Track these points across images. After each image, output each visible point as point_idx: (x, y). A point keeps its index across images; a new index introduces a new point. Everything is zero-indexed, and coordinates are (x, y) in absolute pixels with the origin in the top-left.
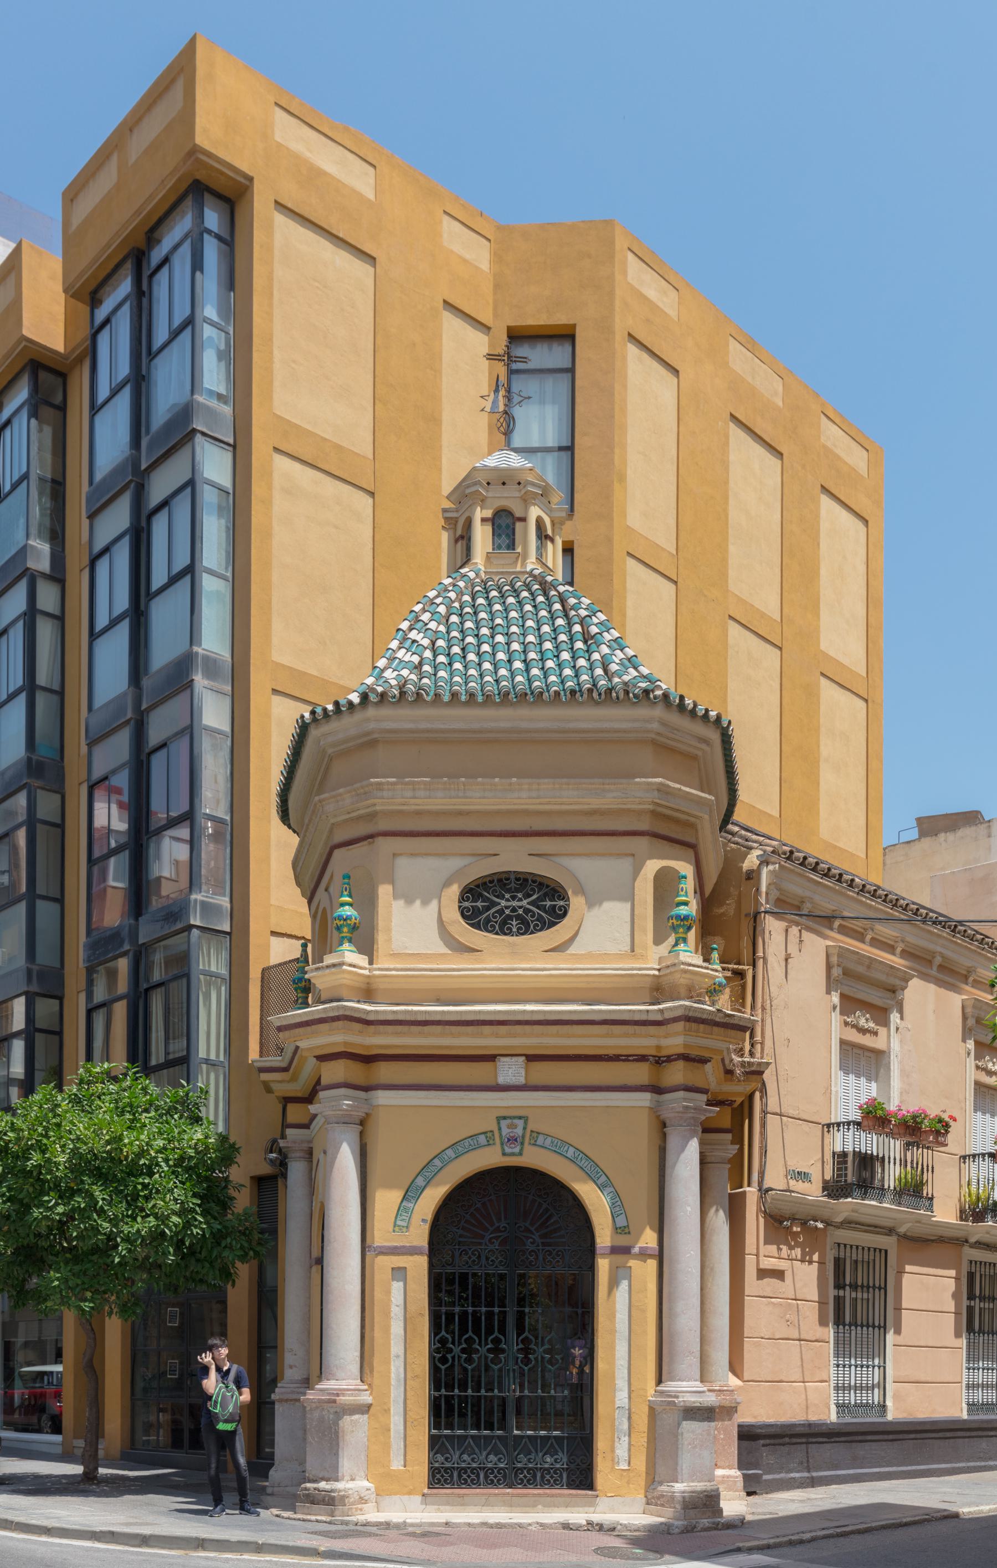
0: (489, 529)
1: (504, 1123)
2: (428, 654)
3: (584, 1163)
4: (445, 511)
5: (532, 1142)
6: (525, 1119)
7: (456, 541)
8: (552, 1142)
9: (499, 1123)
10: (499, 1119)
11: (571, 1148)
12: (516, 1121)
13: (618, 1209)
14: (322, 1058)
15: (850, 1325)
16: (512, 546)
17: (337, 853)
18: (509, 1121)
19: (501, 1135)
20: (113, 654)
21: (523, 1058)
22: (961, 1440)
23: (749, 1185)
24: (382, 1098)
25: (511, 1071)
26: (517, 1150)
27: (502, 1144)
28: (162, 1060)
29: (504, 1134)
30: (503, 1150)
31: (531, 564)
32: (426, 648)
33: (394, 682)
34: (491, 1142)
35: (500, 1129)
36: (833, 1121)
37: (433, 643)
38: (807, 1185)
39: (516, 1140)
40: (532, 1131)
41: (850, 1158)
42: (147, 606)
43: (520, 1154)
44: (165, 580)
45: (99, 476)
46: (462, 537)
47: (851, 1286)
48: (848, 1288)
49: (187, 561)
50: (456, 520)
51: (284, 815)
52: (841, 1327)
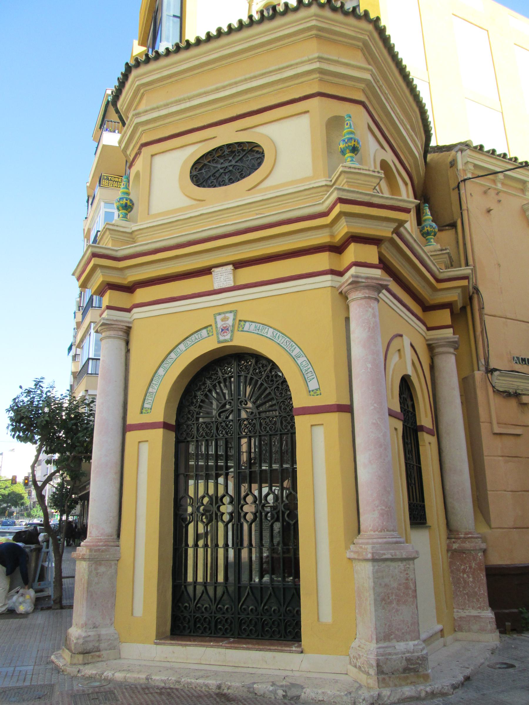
1: (219, 318)
3: (281, 340)
5: (240, 329)
6: (235, 312)
8: (256, 327)
10: (215, 315)
12: (228, 315)
13: (310, 375)
18: (222, 316)
19: (217, 327)
21: (231, 267)
22: (474, 236)
26: (228, 337)
27: (217, 334)
29: (219, 326)
30: (218, 338)
34: (210, 334)
35: (216, 323)
39: (228, 329)
40: (240, 321)
43: (231, 340)
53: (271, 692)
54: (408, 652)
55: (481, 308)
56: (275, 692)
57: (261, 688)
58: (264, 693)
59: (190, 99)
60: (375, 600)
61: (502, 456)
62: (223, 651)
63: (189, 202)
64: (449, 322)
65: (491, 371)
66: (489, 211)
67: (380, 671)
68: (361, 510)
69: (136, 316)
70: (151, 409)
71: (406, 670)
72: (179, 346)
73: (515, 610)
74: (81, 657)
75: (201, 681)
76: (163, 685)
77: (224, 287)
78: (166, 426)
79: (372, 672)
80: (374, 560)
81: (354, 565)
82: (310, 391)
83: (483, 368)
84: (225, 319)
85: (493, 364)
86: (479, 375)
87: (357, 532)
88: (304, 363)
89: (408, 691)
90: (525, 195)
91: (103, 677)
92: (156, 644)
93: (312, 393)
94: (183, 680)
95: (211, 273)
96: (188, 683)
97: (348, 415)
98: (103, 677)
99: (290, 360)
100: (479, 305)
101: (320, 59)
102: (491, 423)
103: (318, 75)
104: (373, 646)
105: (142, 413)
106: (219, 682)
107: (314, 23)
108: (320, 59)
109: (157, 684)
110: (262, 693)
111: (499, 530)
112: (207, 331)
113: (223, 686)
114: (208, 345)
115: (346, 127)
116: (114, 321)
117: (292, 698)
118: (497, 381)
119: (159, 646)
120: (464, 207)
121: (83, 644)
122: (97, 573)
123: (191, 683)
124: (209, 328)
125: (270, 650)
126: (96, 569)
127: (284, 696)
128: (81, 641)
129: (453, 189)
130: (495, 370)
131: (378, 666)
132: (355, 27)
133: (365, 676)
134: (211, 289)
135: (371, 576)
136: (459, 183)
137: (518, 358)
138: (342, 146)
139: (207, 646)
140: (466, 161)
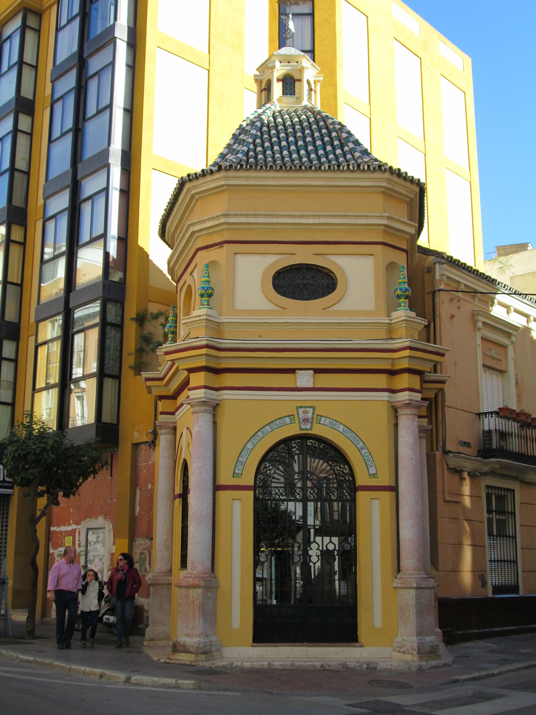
0: (281, 84)
1: (300, 410)
2: (252, 146)
3: (350, 435)
4: (255, 76)
5: (318, 422)
6: (314, 408)
7: (262, 91)
8: (330, 422)
9: (297, 410)
10: (297, 408)
11: (341, 425)
12: (308, 409)
13: (370, 463)
14: (191, 371)
15: (496, 536)
16: (293, 93)
17: (200, 253)
18: (303, 409)
19: (299, 418)
20: (63, 149)
23: (437, 450)
24: (226, 395)
25: (304, 379)
26: (309, 427)
27: (300, 423)
28: (44, 385)
29: (300, 417)
31: (305, 102)
32: (250, 143)
33: (235, 160)
34: (293, 422)
35: (298, 414)
36: (481, 412)
37: (254, 141)
38: (469, 449)
40: (317, 415)
41: (494, 434)
42: (83, 125)
43: (311, 429)
44: (59, 135)
45: (58, 62)
46: (265, 89)
47: (496, 512)
48: (494, 513)
49: (108, 102)
50: (261, 82)
51: (163, 234)
52: (492, 537)
53: (359, 666)
54: (432, 642)
55: (443, 401)
56: (361, 666)
57: (350, 664)
58: (354, 667)
59: (277, 216)
60: (416, 612)
61: (448, 518)
62: (305, 648)
63: (269, 306)
64: (425, 414)
65: (446, 452)
66: (452, 317)
67: (419, 653)
68: (402, 557)
69: (226, 397)
70: (241, 474)
71: (430, 652)
72: (266, 427)
73: (449, 629)
74: (203, 656)
75: (309, 664)
76: (282, 668)
77: (305, 386)
78: (254, 488)
79: (415, 653)
80: (417, 588)
81: (398, 592)
82: (370, 475)
83: (440, 449)
84: (305, 412)
85: (448, 448)
86: (438, 454)
87: (396, 571)
88: (366, 454)
89: (433, 663)
90: (475, 301)
91: (234, 666)
92: (252, 646)
93: (371, 476)
94: (296, 664)
95: (294, 373)
96: (300, 665)
97: (394, 493)
98: (234, 666)
99: (357, 450)
100: (442, 399)
101: (389, 218)
102: (443, 493)
103: (383, 228)
104: (415, 638)
105: (233, 476)
106: (322, 663)
107: (384, 184)
108: (389, 218)
109: (277, 667)
110: (353, 667)
111: (444, 572)
112: (290, 419)
113: (325, 666)
114: (293, 430)
115: (402, 277)
116: (211, 399)
117: (372, 669)
118: (451, 461)
119: (255, 648)
120: (437, 313)
121: (204, 647)
122: (207, 597)
123: (302, 665)
124: (292, 417)
125: (341, 646)
126: (206, 594)
127: (367, 668)
128: (202, 645)
129: (428, 293)
130: (450, 452)
131: (418, 649)
132: (409, 189)
133: (410, 656)
134: (294, 386)
135: (414, 597)
136: (435, 291)
137: (462, 441)
138: (399, 292)
139: (294, 646)
140: (442, 273)
